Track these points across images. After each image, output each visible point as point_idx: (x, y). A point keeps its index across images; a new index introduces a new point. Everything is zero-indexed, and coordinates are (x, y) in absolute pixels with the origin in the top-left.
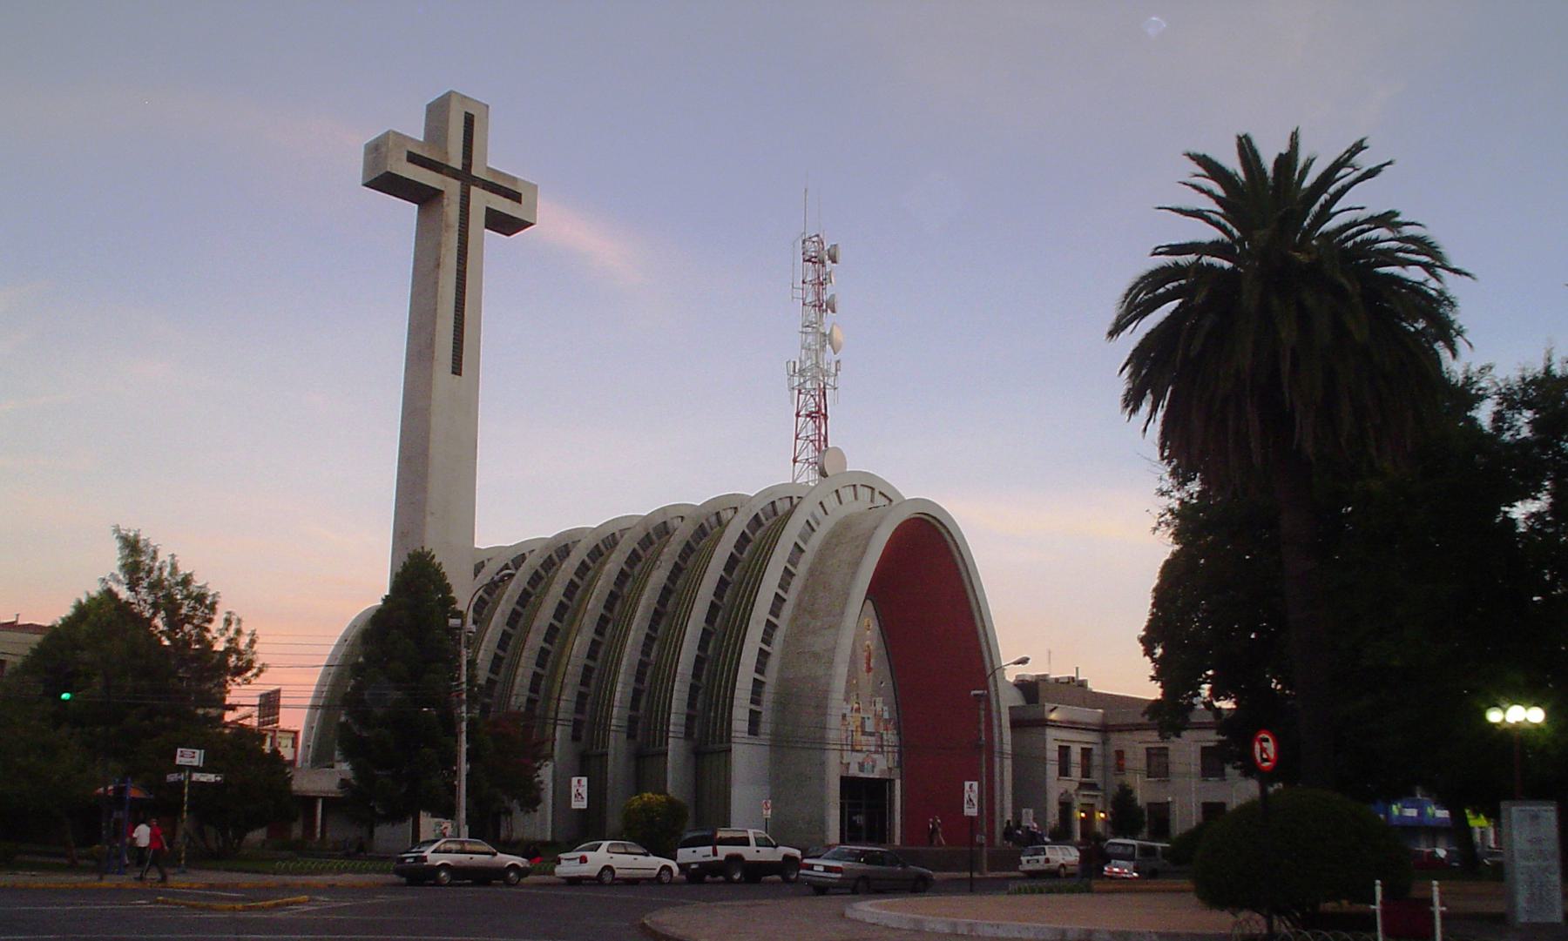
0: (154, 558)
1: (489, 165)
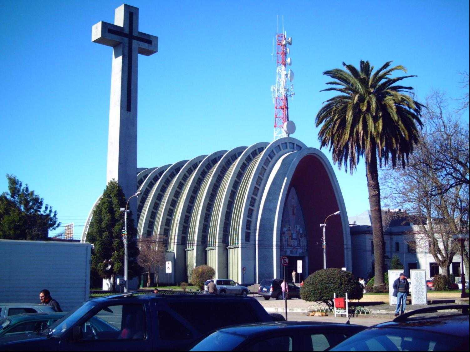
0: (21, 186)
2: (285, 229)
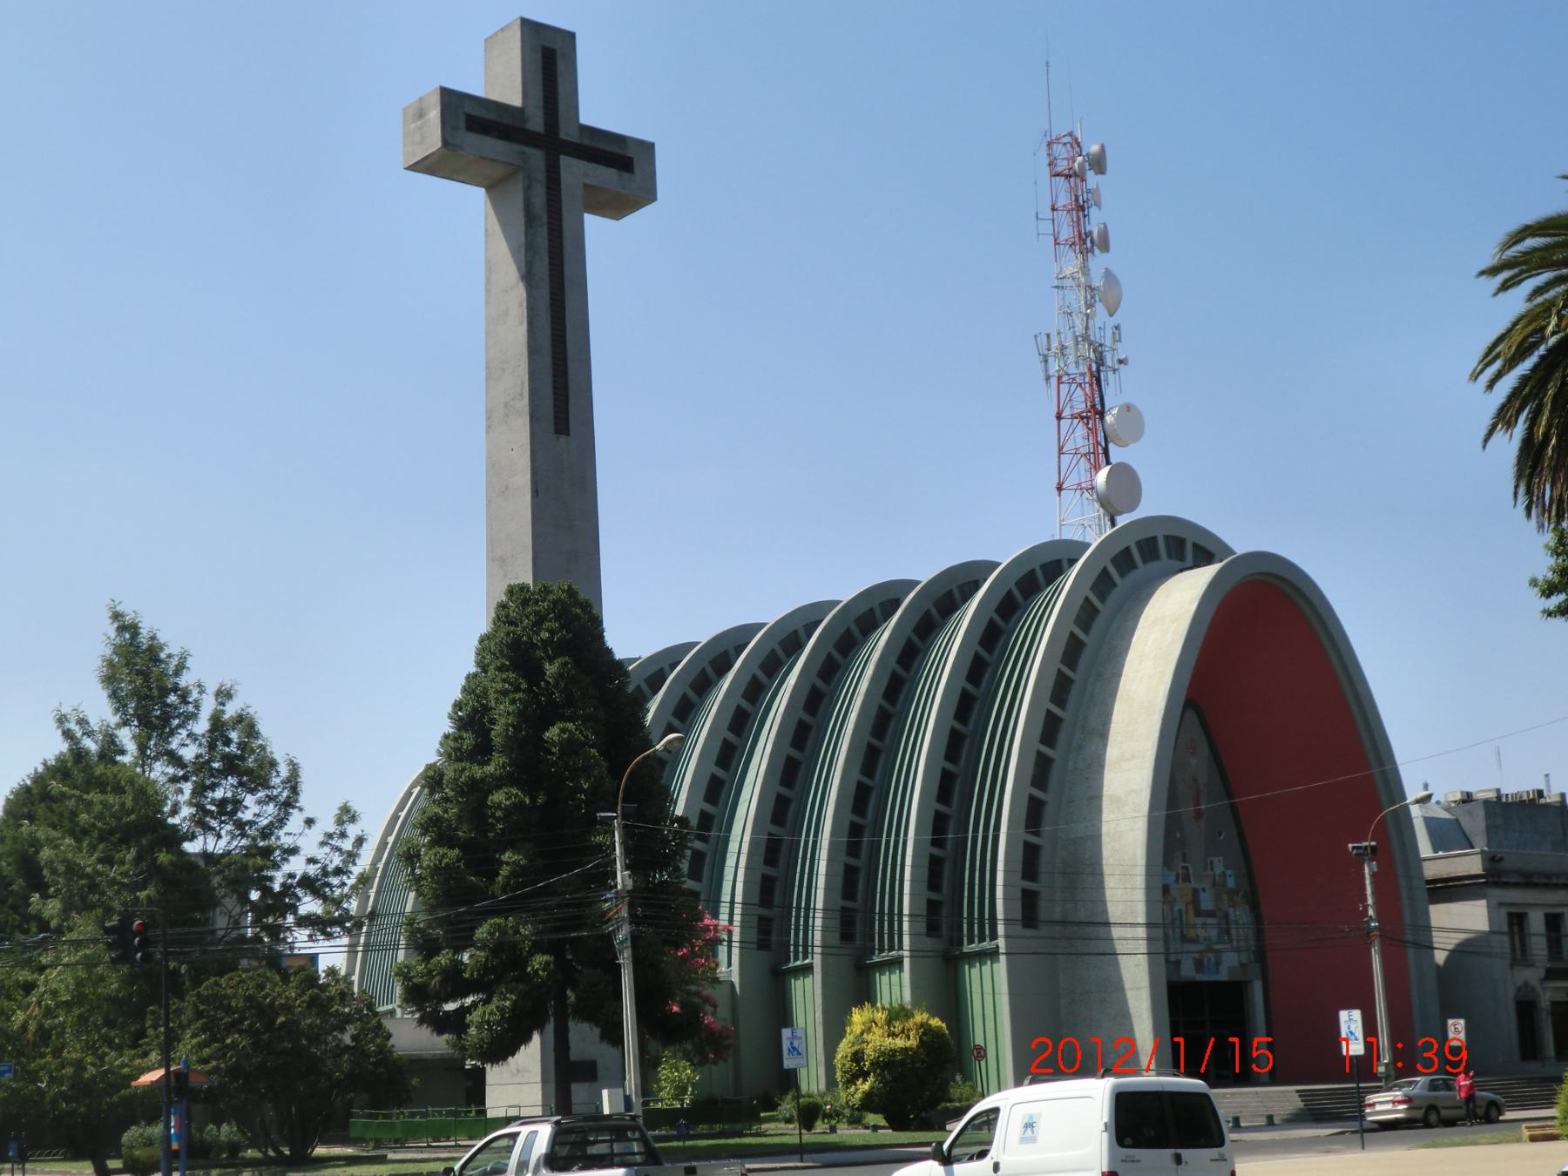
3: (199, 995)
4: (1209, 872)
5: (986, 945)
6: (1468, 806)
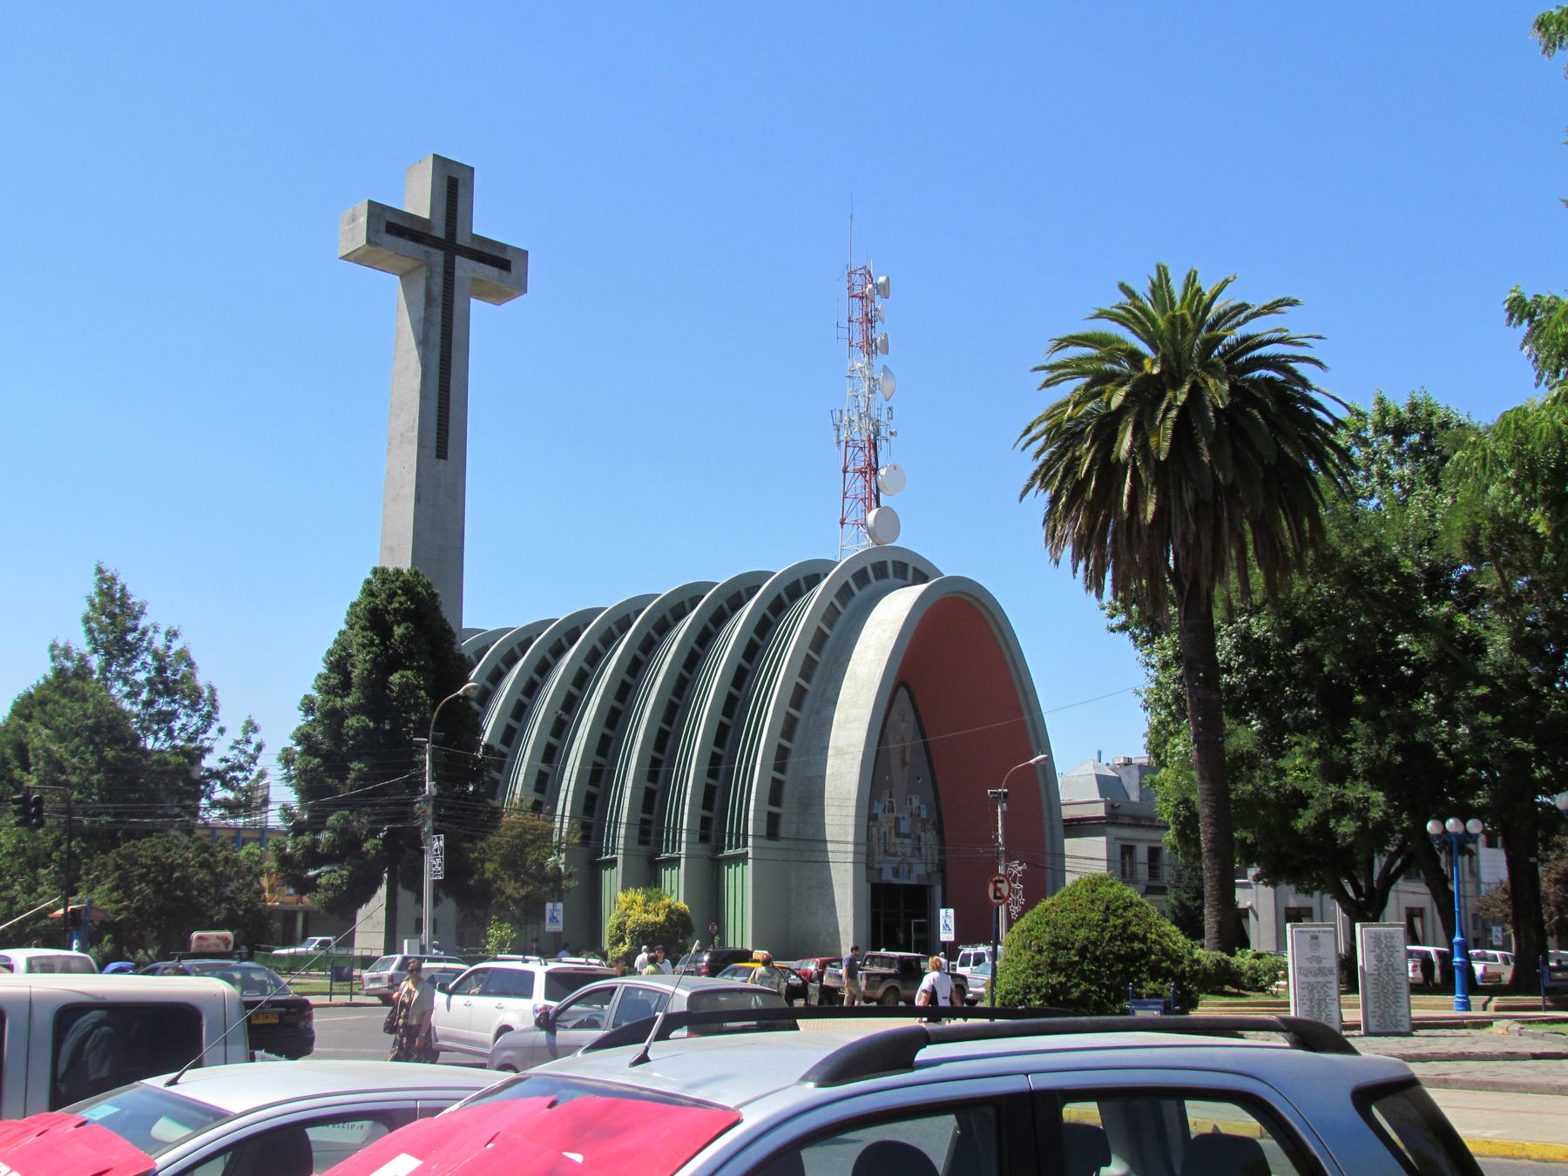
1: (474, 232)
2: (878, 809)
3: (119, 854)
4: (909, 806)
5: (739, 851)
6: (1127, 768)
